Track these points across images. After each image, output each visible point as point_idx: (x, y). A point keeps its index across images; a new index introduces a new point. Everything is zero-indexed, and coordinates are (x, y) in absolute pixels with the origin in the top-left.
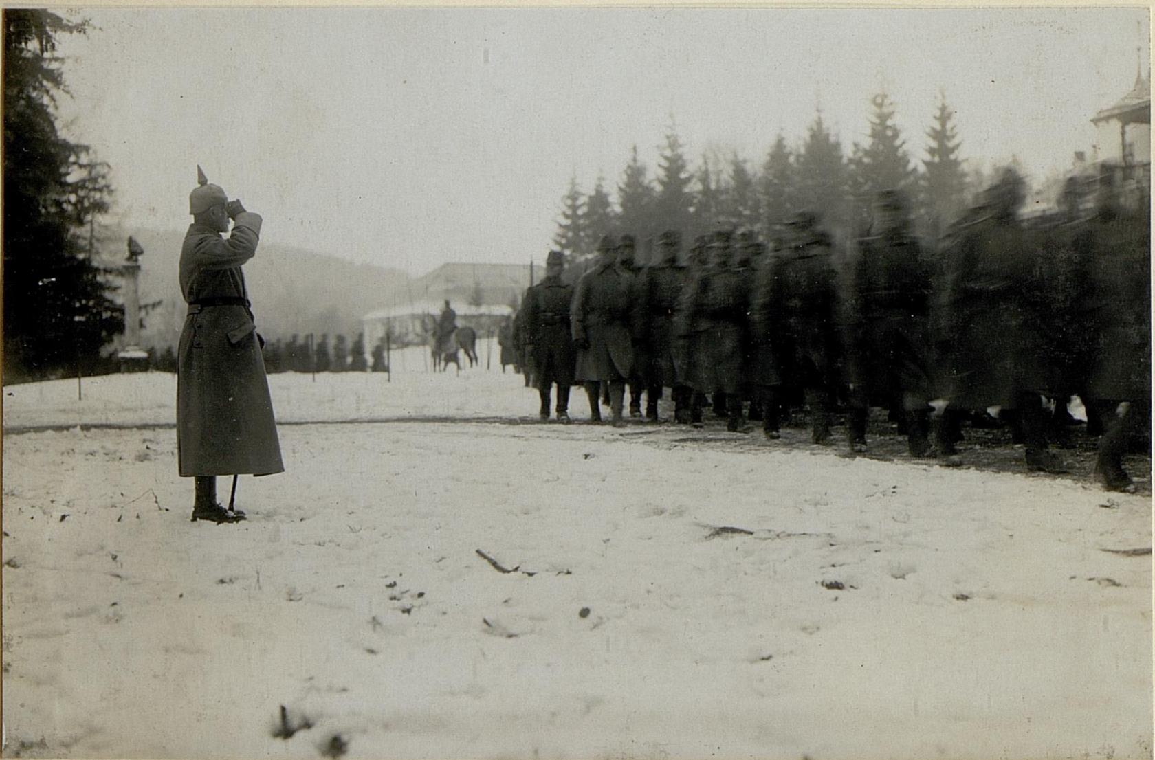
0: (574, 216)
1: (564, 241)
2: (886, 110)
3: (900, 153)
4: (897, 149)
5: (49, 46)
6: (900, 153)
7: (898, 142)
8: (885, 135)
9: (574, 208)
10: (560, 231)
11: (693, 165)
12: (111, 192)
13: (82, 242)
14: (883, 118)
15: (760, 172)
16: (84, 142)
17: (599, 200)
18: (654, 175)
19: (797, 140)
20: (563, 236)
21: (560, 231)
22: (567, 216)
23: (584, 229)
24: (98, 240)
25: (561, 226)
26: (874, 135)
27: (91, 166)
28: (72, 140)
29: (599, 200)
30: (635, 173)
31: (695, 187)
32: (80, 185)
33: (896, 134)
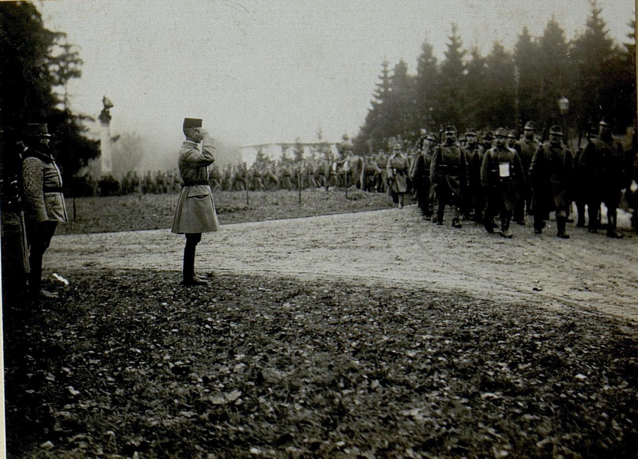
0: (385, 78)
1: (378, 95)
2: (598, 7)
3: (606, 37)
4: (604, 34)
5: (351, 165)
6: (606, 37)
7: (604, 30)
8: (596, 25)
9: (385, 72)
10: (376, 88)
11: (466, 45)
12: (82, 63)
13: (61, 98)
14: (596, 13)
15: (512, 52)
16: (61, 30)
17: (401, 68)
18: (440, 56)
19: (537, 32)
20: (378, 91)
21: (376, 88)
22: (380, 78)
23: (391, 86)
24: (70, 96)
25: (377, 84)
26: (589, 24)
27: (67, 47)
28: (52, 30)
29: (401, 68)
30: (427, 50)
31: (468, 58)
32: (63, 58)
33: (603, 25)
